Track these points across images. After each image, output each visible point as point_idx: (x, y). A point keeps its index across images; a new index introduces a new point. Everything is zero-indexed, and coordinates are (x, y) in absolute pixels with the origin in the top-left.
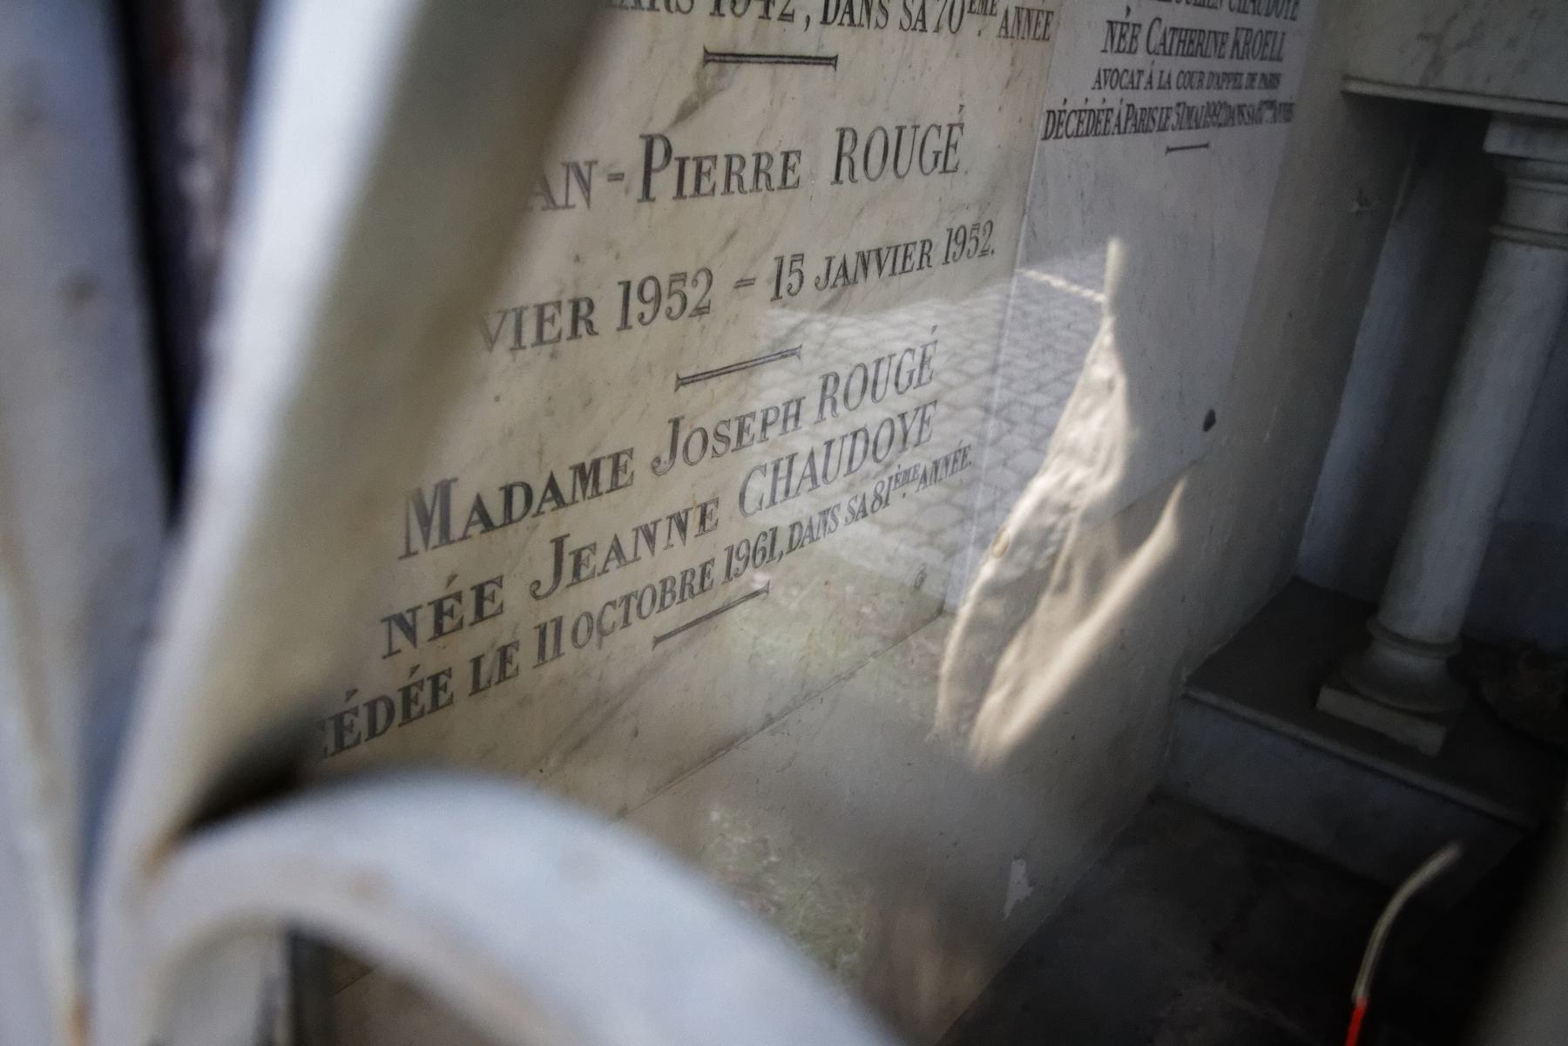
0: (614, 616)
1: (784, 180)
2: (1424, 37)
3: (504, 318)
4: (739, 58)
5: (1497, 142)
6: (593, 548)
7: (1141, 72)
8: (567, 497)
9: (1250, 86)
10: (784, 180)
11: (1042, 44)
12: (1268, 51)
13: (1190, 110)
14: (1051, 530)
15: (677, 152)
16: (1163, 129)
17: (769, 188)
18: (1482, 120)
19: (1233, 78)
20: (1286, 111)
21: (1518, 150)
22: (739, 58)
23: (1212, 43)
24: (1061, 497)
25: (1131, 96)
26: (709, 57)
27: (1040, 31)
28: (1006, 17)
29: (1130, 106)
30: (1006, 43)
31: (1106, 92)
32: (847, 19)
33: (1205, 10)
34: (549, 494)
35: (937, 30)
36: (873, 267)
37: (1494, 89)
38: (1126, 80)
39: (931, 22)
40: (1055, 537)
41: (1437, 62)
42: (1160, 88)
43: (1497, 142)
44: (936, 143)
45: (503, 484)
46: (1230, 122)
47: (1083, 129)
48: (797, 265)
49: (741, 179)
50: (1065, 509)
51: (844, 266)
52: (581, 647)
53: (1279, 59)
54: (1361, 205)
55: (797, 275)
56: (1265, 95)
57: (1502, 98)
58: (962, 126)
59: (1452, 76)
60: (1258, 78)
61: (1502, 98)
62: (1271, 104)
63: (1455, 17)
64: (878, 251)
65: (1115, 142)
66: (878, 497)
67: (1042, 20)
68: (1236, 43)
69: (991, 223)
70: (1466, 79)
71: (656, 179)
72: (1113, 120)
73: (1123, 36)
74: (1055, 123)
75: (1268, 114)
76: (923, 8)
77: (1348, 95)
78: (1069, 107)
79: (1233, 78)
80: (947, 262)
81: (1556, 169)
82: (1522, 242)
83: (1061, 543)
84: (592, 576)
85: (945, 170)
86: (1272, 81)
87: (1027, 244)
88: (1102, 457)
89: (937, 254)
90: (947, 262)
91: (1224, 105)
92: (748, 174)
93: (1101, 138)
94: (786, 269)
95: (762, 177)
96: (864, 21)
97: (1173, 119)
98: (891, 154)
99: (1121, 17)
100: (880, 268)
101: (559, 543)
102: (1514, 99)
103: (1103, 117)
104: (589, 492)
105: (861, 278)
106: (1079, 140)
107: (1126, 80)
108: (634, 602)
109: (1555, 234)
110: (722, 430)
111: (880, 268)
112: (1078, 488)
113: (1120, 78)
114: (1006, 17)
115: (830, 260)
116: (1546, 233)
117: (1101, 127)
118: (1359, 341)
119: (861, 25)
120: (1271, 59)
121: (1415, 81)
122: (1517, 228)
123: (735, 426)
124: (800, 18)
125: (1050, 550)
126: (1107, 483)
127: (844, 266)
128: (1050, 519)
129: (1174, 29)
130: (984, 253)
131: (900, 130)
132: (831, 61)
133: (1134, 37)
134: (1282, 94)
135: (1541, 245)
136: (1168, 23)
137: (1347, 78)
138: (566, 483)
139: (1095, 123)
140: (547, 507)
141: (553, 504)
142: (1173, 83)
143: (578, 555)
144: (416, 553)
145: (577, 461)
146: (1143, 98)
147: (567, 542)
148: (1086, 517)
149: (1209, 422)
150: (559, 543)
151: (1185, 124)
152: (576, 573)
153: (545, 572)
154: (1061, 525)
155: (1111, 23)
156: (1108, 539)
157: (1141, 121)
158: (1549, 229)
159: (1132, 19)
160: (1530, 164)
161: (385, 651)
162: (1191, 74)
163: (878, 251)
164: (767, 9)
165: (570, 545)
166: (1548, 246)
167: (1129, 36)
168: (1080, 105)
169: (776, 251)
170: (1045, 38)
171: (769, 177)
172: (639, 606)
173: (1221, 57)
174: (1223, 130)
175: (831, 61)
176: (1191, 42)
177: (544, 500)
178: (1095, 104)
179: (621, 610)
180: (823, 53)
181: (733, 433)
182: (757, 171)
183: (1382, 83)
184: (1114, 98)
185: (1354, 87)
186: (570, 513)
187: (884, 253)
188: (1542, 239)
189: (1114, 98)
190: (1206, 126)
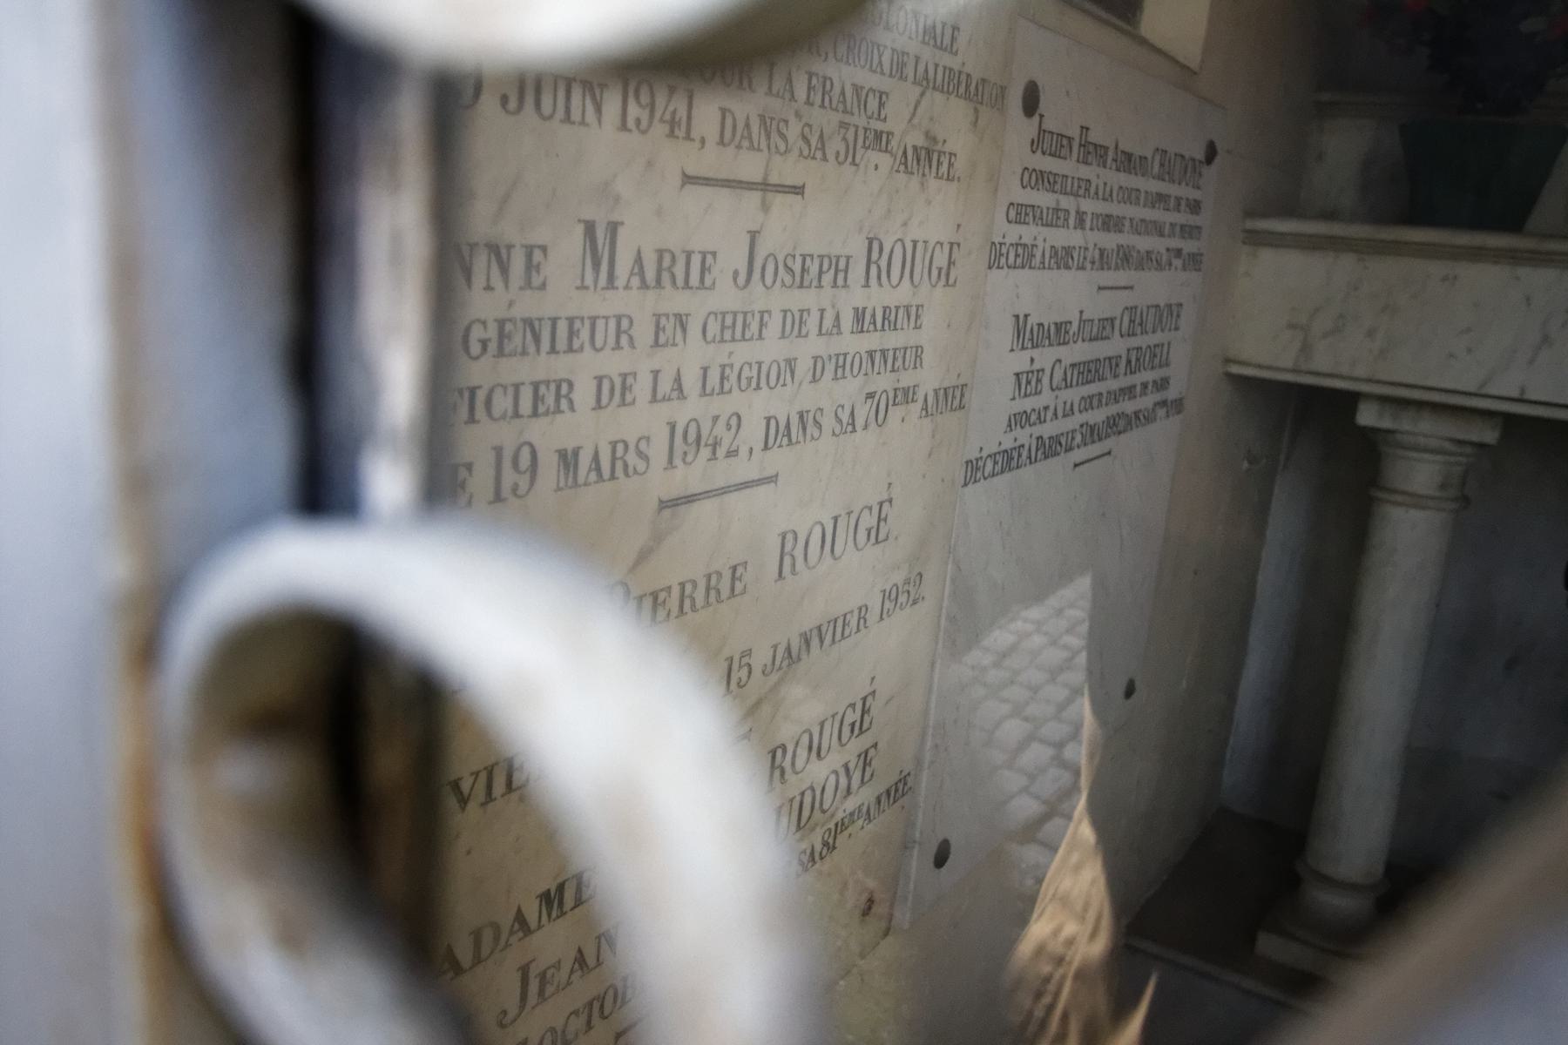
0: (577, 1023)
1: (733, 589)
2: (1292, 326)
4: (690, 499)
5: (1367, 416)
6: (557, 965)
7: (1046, 408)
8: (533, 924)
9: (1144, 393)
10: (733, 589)
11: (959, 414)
12: (1157, 361)
13: (1092, 428)
14: (1047, 979)
16: (1069, 449)
17: (719, 601)
18: (1348, 401)
19: (1129, 392)
20: (1177, 406)
21: (1386, 423)
22: (690, 499)
23: (1107, 370)
24: (1056, 947)
25: (1038, 430)
26: (663, 505)
27: (956, 403)
29: (1040, 438)
30: (927, 421)
31: (1018, 432)
32: (785, 440)
33: (1100, 343)
34: (517, 926)
35: (866, 427)
36: (815, 642)
37: (1361, 371)
38: (1033, 417)
39: (860, 422)
40: (1051, 987)
41: (1306, 349)
43: (1367, 416)
44: (869, 520)
46: (1129, 426)
47: (998, 468)
48: (745, 660)
49: (693, 600)
50: (1060, 961)
51: (788, 649)
53: (1167, 365)
54: (1250, 463)
55: (745, 670)
56: (1158, 397)
57: (1369, 381)
58: (890, 501)
61: (1369, 381)
62: (1164, 403)
64: (819, 628)
65: (1027, 473)
66: (826, 844)
67: (958, 394)
68: (1129, 362)
69: (920, 575)
70: (1339, 361)
72: (1025, 453)
73: (1028, 382)
74: (974, 470)
75: (1161, 412)
76: (852, 413)
77: (1229, 376)
78: (984, 454)
79: (1129, 392)
80: (882, 618)
81: (1422, 440)
83: (1057, 994)
84: (557, 991)
85: (877, 542)
86: (1162, 384)
87: (953, 581)
88: (1091, 915)
89: (873, 617)
90: (882, 618)
91: (1121, 415)
92: (700, 596)
93: (1014, 472)
94: (735, 666)
95: (713, 593)
96: (801, 438)
97: (1078, 438)
98: (862, 619)
99: (1027, 368)
100: (822, 641)
101: (524, 971)
102: (1378, 382)
103: (1015, 454)
104: (554, 914)
105: (804, 656)
106: (995, 479)
107: (1033, 417)
108: (596, 1005)
109: (1427, 497)
111: (822, 641)
112: (1070, 942)
113: (1028, 418)
115: (775, 647)
116: (1421, 496)
117: (1014, 463)
118: (1260, 578)
120: (1161, 366)
121: (1289, 364)
122: (1395, 491)
124: (744, 451)
125: (1047, 1000)
126: (1097, 948)
127: (788, 649)
128: (1046, 969)
129: (1073, 365)
130: (915, 603)
131: (836, 519)
132: (772, 479)
133: (1039, 380)
134: (1172, 394)
135: (1415, 506)
136: (1067, 361)
137: (1228, 361)
138: (532, 911)
139: (1008, 460)
140: (513, 939)
141: (521, 934)
142: (1076, 408)
143: (543, 977)
145: (542, 888)
146: (1048, 429)
147: (533, 966)
148: (1079, 976)
149: (1130, 691)
150: (524, 971)
151: (1088, 439)
152: (541, 992)
154: (1057, 976)
155: (1017, 375)
156: (1101, 1001)
157: (1050, 448)
159: (1037, 366)
160: (1399, 437)
162: (1091, 397)
163: (819, 628)
164: (714, 453)
165: (534, 971)
166: (1423, 508)
168: (995, 449)
169: (726, 653)
170: (961, 407)
171: (718, 592)
172: (602, 1007)
173: (1116, 376)
175: (772, 479)
177: (512, 933)
178: (1008, 444)
179: (583, 1018)
182: (708, 589)
183: (1260, 366)
184: (1024, 436)
185: (1235, 369)
186: (536, 939)
187: (824, 629)
189: (1024, 436)
190: (1108, 436)
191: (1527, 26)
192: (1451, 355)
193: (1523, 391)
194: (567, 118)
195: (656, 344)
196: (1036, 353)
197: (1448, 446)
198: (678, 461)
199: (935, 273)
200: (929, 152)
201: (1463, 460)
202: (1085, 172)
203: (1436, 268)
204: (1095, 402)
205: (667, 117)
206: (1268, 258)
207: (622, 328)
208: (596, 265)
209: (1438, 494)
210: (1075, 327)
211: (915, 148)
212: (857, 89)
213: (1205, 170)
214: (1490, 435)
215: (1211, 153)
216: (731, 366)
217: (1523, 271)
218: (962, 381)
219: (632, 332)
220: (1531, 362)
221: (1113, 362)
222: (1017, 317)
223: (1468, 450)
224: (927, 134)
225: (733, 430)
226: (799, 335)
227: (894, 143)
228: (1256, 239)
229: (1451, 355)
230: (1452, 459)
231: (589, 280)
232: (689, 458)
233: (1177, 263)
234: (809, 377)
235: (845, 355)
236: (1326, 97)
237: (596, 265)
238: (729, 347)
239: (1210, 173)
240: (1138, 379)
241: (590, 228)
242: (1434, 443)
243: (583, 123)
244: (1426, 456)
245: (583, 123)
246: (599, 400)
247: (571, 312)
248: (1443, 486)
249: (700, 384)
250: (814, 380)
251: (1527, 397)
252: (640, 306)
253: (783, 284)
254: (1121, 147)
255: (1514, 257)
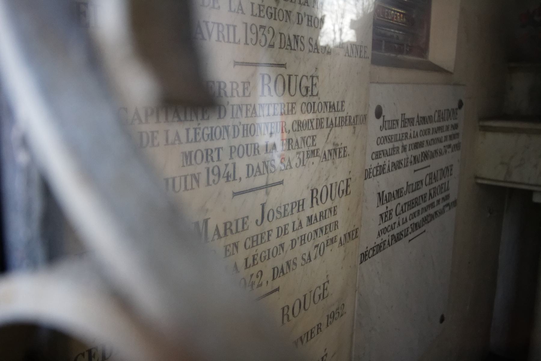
15: (242, 123)
25: (391, 233)
28: (341, 240)
42: (414, 137)
52: (243, 278)
59: (515, 178)
60: (450, 127)
62: (448, 205)
71: (233, 155)
77: (478, 184)
86: (448, 197)
91: (430, 215)
110: (279, 209)
114: (341, 240)
123: (283, 208)
129: (405, 204)
132: (278, 289)
137: (477, 177)
149: (442, 320)
167: (388, 216)
174: (430, 223)
176: (413, 203)
180: (274, 289)
181: (282, 211)
183: (489, 180)
185: (479, 181)
204: (416, 214)
206: (490, 136)
243: (192, 188)
245: (192, 188)
246: (248, 174)
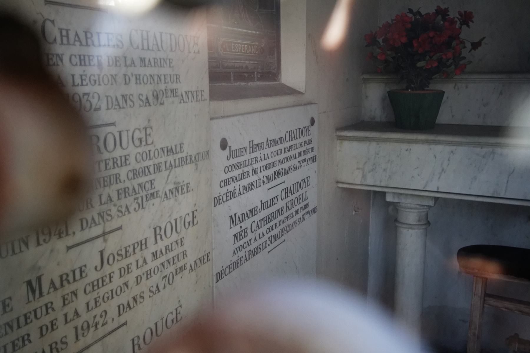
2: (358, 169)
3: (41, 309)
5: (389, 198)
21: (396, 200)
37: (383, 184)
41: (364, 177)
43: (389, 198)
45: (64, 288)
59: (370, 181)
62: (308, 212)
63: (366, 162)
70: (374, 180)
78: (224, 268)
82: (406, 228)
96: (135, 305)
101: (102, 253)
116: (410, 225)
119: (186, 102)
129: (261, 220)
132: (125, 324)
135: (411, 228)
137: (338, 182)
144: (31, 301)
150: (102, 253)
153: (98, 262)
155: (235, 235)
158: (412, 223)
161: (27, 302)
185: (340, 185)
188: (410, 226)
191: (420, 64)
192: (413, 177)
193: (438, 188)
194: (14, 252)
195: (64, 304)
196: (242, 224)
197: (418, 206)
198: (80, 337)
199: (187, 224)
200: (177, 188)
201: (425, 210)
202: (253, 155)
203: (405, 146)
205: (57, 233)
207: (48, 307)
208: (33, 292)
209: (417, 223)
210: (259, 207)
211: (170, 190)
212: (140, 185)
213: (312, 128)
214: (431, 203)
215: (313, 122)
216: (99, 297)
217: (432, 146)
218: (206, 253)
219: (53, 306)
220: (439, 178)
221: (280, 211)
222: (231, 216)
223: (426, 207)
224: (175, 183)
225: (104, 317)
226: (128, 273)
227: (160, 193)
228: (343, 139)
229: (413, 177)
230: (421, 210)
231: (31, 298)
232: (85, 334)
233: (305, 163)
234: (136, 283)
235: (150, 270)
236: (365, 76)
237: (33, 292)
238: (96, 292)
239: (314, 129)
240: (293, 211)
241: (29, 283)
242: (413, 206)
244: (413, 210)
247: (25, 312)
248: (419, 221)
249: (86, 308)
250: (138, 284)
251: (440, 190)
252: (56, 298)
253: (118, 260)
254: (269, 139)
255: (427, 142)
